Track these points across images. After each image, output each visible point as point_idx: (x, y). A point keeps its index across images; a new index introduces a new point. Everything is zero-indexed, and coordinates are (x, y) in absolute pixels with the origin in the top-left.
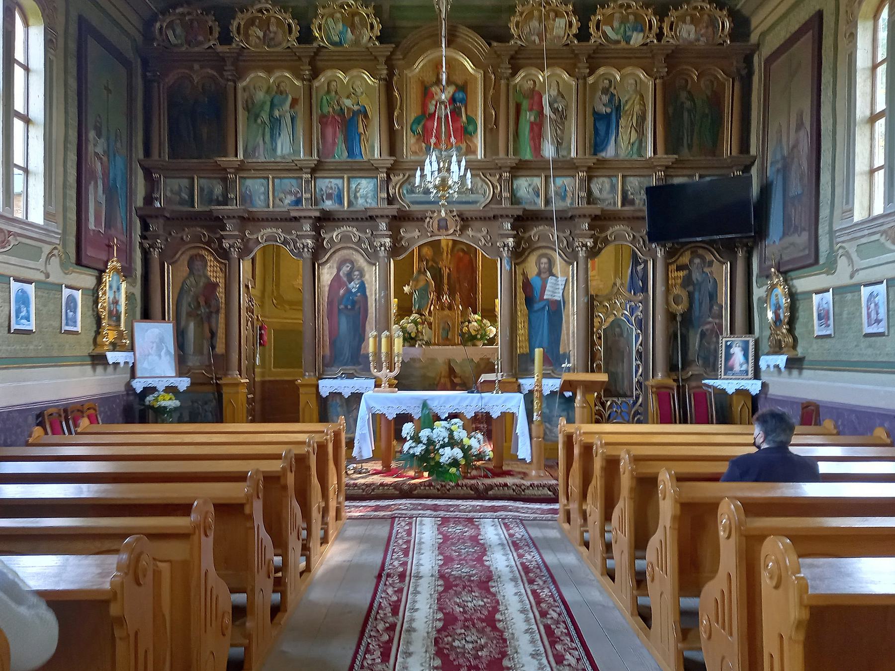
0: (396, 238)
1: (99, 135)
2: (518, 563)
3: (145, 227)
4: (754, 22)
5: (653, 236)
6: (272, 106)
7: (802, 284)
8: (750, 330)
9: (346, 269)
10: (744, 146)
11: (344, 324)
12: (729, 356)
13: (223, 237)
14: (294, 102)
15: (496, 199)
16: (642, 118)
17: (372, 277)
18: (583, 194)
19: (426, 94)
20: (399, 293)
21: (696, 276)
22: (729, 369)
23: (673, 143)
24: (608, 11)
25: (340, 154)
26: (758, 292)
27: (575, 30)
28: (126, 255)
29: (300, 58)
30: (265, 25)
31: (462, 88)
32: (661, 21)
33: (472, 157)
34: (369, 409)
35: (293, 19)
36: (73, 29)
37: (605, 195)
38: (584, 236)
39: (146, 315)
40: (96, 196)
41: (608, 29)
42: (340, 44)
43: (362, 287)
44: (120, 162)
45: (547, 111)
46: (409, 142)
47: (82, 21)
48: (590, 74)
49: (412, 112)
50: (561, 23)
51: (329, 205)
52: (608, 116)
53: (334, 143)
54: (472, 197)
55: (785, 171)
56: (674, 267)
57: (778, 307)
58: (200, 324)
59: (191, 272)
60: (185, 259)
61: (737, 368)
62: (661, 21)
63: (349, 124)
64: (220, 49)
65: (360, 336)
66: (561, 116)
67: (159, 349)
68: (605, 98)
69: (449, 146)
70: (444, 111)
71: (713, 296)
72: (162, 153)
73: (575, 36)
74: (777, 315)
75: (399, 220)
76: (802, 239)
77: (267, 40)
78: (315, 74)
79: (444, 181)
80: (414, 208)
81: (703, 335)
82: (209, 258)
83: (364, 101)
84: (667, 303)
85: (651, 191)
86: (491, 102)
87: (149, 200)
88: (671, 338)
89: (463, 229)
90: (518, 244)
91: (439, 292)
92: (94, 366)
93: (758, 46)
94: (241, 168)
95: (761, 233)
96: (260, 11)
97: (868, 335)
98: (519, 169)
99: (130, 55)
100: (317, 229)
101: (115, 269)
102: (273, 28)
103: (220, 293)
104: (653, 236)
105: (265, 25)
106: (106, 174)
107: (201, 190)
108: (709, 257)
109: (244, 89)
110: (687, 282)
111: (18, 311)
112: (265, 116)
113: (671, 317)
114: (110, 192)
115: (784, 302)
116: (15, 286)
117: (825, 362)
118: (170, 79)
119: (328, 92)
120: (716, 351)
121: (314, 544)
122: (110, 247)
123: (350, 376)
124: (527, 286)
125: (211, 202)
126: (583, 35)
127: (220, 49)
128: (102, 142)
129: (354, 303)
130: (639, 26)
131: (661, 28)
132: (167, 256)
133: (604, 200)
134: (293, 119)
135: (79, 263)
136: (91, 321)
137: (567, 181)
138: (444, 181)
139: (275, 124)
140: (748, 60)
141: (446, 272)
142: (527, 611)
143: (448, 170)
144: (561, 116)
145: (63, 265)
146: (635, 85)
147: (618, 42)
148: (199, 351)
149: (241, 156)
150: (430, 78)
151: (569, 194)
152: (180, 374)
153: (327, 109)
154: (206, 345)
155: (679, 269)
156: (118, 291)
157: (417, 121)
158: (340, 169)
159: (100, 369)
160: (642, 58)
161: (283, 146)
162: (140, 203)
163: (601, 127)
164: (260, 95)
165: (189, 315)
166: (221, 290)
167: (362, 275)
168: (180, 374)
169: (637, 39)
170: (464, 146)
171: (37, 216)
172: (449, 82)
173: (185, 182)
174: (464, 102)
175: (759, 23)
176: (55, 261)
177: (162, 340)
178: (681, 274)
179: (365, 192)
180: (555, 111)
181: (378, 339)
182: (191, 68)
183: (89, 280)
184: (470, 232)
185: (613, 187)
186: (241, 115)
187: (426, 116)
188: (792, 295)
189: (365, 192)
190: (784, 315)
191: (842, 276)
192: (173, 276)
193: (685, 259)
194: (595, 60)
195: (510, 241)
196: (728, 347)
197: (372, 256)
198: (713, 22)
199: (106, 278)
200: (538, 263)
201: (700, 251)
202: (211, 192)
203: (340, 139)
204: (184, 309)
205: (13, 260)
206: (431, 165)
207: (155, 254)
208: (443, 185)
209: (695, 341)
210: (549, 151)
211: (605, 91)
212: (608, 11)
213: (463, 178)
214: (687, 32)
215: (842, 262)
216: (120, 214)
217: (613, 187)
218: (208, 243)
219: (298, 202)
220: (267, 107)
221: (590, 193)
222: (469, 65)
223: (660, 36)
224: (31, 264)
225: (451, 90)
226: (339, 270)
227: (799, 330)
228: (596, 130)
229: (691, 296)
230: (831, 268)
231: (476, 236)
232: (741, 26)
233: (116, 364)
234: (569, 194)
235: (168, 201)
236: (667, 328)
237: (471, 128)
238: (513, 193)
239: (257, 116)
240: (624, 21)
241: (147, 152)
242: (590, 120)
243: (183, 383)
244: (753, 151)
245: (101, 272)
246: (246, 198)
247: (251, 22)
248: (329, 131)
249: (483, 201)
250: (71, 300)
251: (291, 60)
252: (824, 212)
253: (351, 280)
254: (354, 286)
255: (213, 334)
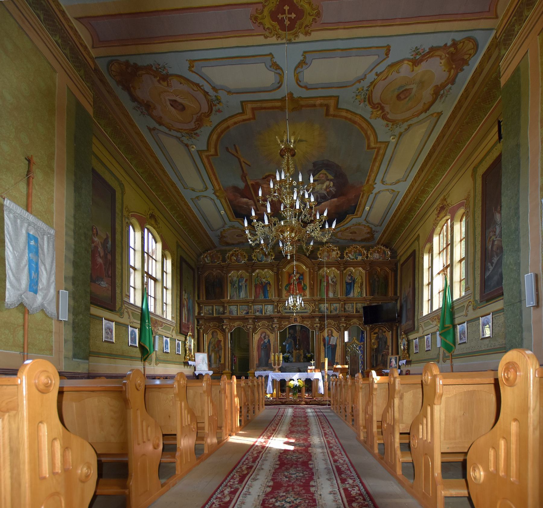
0: (280, 325)
1: (186, 293)
2: (329, 451)
3: (198, 322)
4: (399, 252)
5: (366, 323)
6: (239, 282)
7: (411, 337)
8: (398, 354)
9: (263, 335)
10: (395, 293)
11: (263, 353)
12: (391, 362)
13: (223, 325)
14: (246, 280)
15: (314, 311)
16: (362, 284)
17: (272, 337)
18: (343, 309)
19: (290, 276)
20: (281, 344)
21: (380, 336)
22: (391, 366)
23: (372, 293)
24: (350, 249)
25: (262, 297)
26: (400, 341)
27: (339, 255)
28: (193, 332)
29: (248, 266)
30: (237, 256)
31: (302, 275)
32: (368, 252)
33: (305, 297)
34: (272, 377)
35: (246, 253)
36: (179, 260)
37: (350, 309)
38: (343, 323)
39: (199, 351)
40: (185, 312)
41: (350, 255)
42: (261, 261)
43: (269, 341)
44: (191, 301)
45: (330, 282)
46: (284, 292)
47: (181, 258)
48: (344, 270)
49: (285, 283)
50: (334, 253)
51: (258, 314)
52: (350, 283)
53: (259, 294)
54: (305, 311)
55: (406, 301)
56: (372, 333)
57: (404, 345)
58: (216, 354)
59: (213, 337)
60: (210, 332)
61: (393, 366)
62: (368, 252)
63: (264, 287)
64: (222, 264)
65: (268, 356)
66: (335, 283)
67: (203, 362)
68: (350, 278)
69: (297, 295)
70: (296, 283)
71: (386, 342)
72: (203, 298)
73: (339, 257)
74: (404, 347)
75: (282, 318)
76: (410, 322)
77: (237, 261)
78: (253, 271)
79: (295, 304)
80: (286, 314)
81: (383, 356)
82: (219, 332)
83: (269, 279)
84: (370, 344)
85: (364, 308)
86: (312, 279)
87: (199, 313)
88: (372, 357)
89: (303, 321)
90: (321, 326)
91: (295, 344)
92: (184, 365)
93: (399, 260)
94: (228, 302)
95: (400, 322)
96: (235, 251)
97: (427, 351)
98: (321, 301)
99: (194, 267)
100: (254, 322)
101: (190, 335)
102: (239, 257)
103: (222, 343)
104: (366, 323)
105: (237, 256)
106: (187, 305)
107: (216, 310)
108: (385, 330)
109: (230, 276)
110: (377, 338)
111: (165, 346)
112: (237, 285)
113: (372, 349)
114: (188, 310)
115: (406, 343)
116: (165, 338)
117: (417, 361)
118: (206, 274)
119: (257, 277)
120: (387, 361)
121: (257, 410)
122: (188, 328)
123: (265, 370)
124: (324, 340)
125: (219, 313)
126: (342, 257)
127: (222, 264)
128: (186, 294)
129: (266, 346)
130: (360, 254)
131: (367, 255)
132: (205, 332)
133: (349, 311)
134: (246, 286)
135: (180, 333)
136: (184, 351)
137: (338, 305)
138: (295, 304)
139: (240, 288)
140: (396, 265)
141: (298, 338)
142: (332, 479)
143: (296, 301)
144: (335, 283)
145: (176, 333)
146: (359, 273)
147: (353, 259)
148: (216, 363)
149: (229, 298)
150: (291, 271)
151: (338, 309)
152: (210, 370)
153: (257, 283)
154: (218, 360)
155: (375, 334)
156: (192, 343)
157: (287, 286)
158: (261, 302)
159: (186, 367)
160: (362, 264)
161: (243, 295)
162: (196, 314)
163: (350, 286)
164: (235, 279)
165: (212, 351)
166: (222, 343)
167: (269, 337)
168: (210, 370)
169: (360, 258)
170: (302, 294)
171: (169, 318)
172: (297, 273)
173: (211, 307)
174: (303, 279)
175: (400, 252)
176: (174, 331)
177: (204, 359)
178: (375, 335)
179: (269, 309)
180: (333, 282)
181: (274, 356)
182: (213, 270)
183: (183, 339)
184: (305, 322)
185: (353, 307)
186: (229, 285)
187: (289, 284)
188: (409, 341)
189: (269, 309)
190: (406, 347)
191: (420, 334)
192: (206, 338)
193: (376, 331)
194: (347, 264)
195: (318, 325)
196: (391, 359)
197: (272, 330)
198: (384, 252)
199: (188, 338)
200: (328, 332)
201: (382, 328)
202: (219, 310)
203: (261, 291)
204: (211, 349)
205: (164, 331)
206: (291, 299)
207: (201, 331)
208: (294, 305)
209: (380, 358)
210: (331, 295)
211: (350, 275)
212: (350, 249)
213: (301, 303)
214: (376, 256)
215: (421, 329)
216: (191, 318)
217: (353, 307)
218: (218, 327)
219: (247, 313)
220: (237, 282)
221: (345, 309)
222: (304, 267)
223: (367, 257)
224: (168, 332)
225: (298, 275)
226: (261, 335)
227: (411, 352)
228: (346, 287)
229: (378, 342)
230: (418, 331)
231: (307, 324)
232: (394, 253)
233: (191, 365)
234: (338, 309)
235: (205, 313)
236: (370, 353)
237: (305, 288)
238: (319, 309)
239: (234, 285)
240: (355, 252)
241: (199, 298)
242: (345, 285)
243: (211, 373)
244: (398, 295)
245: (186, 336)
246: (231, 312)
247: (232, 255)
248: (258, 290)
249: (309, 312)
250: (178, 344)
251: (245, 267)
252: (416, 314)
253: (265, 339)
254: (266, 341)
255: (220, 357)
